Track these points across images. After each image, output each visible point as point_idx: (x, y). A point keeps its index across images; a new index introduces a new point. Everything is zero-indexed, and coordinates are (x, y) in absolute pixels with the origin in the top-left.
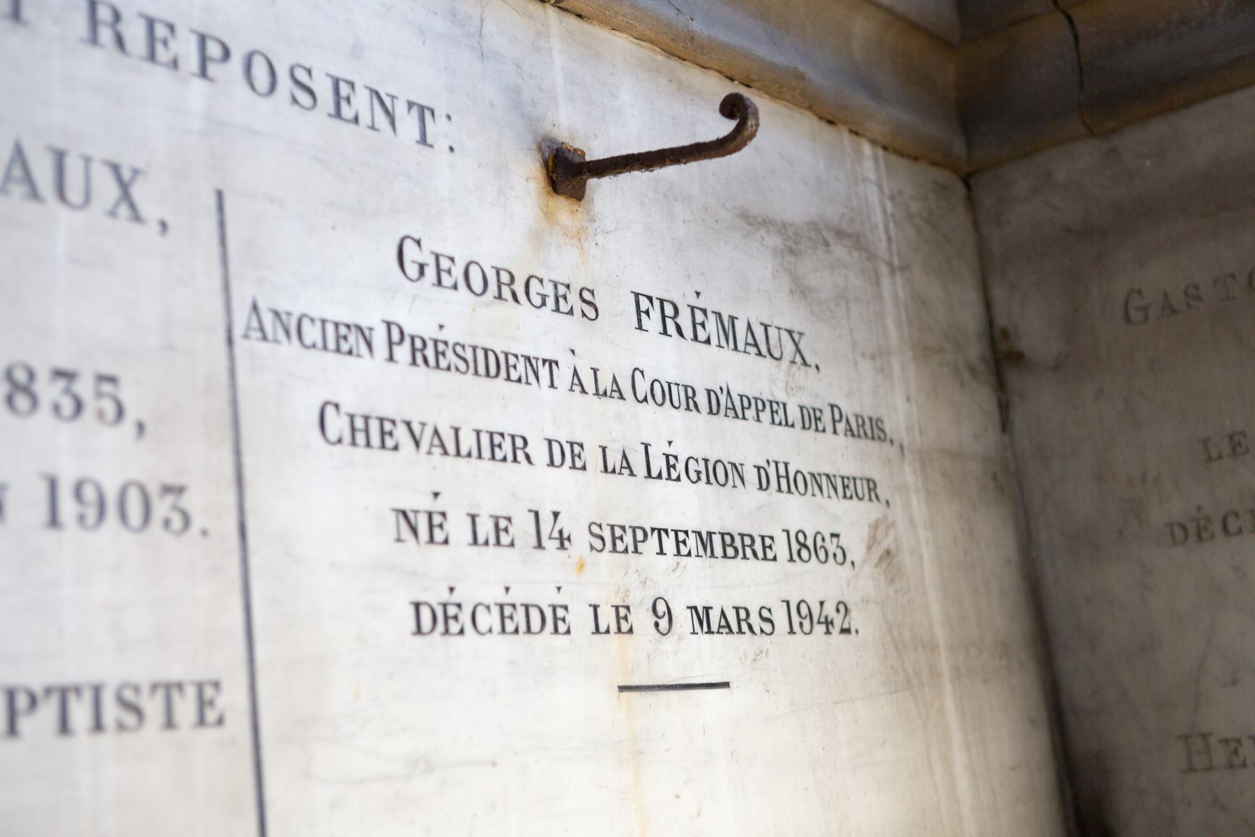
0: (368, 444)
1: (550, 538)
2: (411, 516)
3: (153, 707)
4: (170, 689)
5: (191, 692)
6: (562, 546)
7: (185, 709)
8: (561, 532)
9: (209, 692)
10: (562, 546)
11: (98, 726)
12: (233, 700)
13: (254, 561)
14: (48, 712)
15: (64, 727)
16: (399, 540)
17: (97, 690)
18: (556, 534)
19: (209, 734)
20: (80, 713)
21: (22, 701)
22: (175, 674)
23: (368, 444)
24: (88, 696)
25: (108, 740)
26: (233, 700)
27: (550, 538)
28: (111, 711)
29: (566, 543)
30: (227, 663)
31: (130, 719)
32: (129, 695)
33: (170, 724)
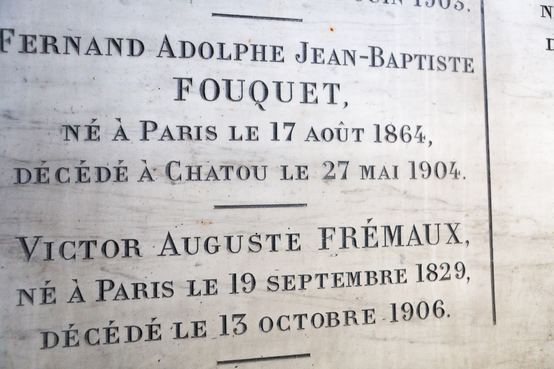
0: (264, 59)
1: (415, 137)
2: (549, 8)
3: (450, 64)
4: (456, 60)
5: (463, 61)
6: (421, 141)
7: (461, 66)
8: (421, 135)
9: (469, 62)
10: (421, 141)
11: (431, 68)
12: (477, 65)
13: (486, 21)
14: (416, 61)
15: (420, 68)
16: (543, 16)
17: (431, 57)
18: (418, 135)
19: (468, 75)
20: (426, 64)
21: (407, 58)
22: (457, 55)
23: (264, 59)
24: (428, 58)
25: (434, 72)
26: (477, 65)
27: (415, 137)
28: (435, 64)
29: (423, 140)
30: (476, 53)
31: (442, 67)
32: (441, 60)
33: (455, 70)
